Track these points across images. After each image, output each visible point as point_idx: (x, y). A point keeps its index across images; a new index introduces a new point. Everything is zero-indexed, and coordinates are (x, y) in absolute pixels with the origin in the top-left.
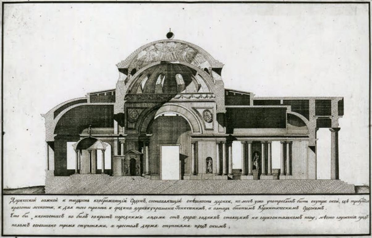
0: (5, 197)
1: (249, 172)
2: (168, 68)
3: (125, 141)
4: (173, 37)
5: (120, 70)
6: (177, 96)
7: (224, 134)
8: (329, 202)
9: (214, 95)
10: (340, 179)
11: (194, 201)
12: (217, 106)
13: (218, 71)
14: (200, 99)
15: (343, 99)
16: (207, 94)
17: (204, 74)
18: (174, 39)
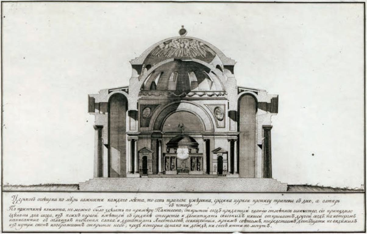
1: (160, 170)
4: (186, 34)
5: (134, 66)
8: (81, 201)
10: (273, 176)
11: (71, 200)
12: (228, 103)
13: (231, 68)
15: (278, 96)
17: (217, 71)
18: (186, 36)
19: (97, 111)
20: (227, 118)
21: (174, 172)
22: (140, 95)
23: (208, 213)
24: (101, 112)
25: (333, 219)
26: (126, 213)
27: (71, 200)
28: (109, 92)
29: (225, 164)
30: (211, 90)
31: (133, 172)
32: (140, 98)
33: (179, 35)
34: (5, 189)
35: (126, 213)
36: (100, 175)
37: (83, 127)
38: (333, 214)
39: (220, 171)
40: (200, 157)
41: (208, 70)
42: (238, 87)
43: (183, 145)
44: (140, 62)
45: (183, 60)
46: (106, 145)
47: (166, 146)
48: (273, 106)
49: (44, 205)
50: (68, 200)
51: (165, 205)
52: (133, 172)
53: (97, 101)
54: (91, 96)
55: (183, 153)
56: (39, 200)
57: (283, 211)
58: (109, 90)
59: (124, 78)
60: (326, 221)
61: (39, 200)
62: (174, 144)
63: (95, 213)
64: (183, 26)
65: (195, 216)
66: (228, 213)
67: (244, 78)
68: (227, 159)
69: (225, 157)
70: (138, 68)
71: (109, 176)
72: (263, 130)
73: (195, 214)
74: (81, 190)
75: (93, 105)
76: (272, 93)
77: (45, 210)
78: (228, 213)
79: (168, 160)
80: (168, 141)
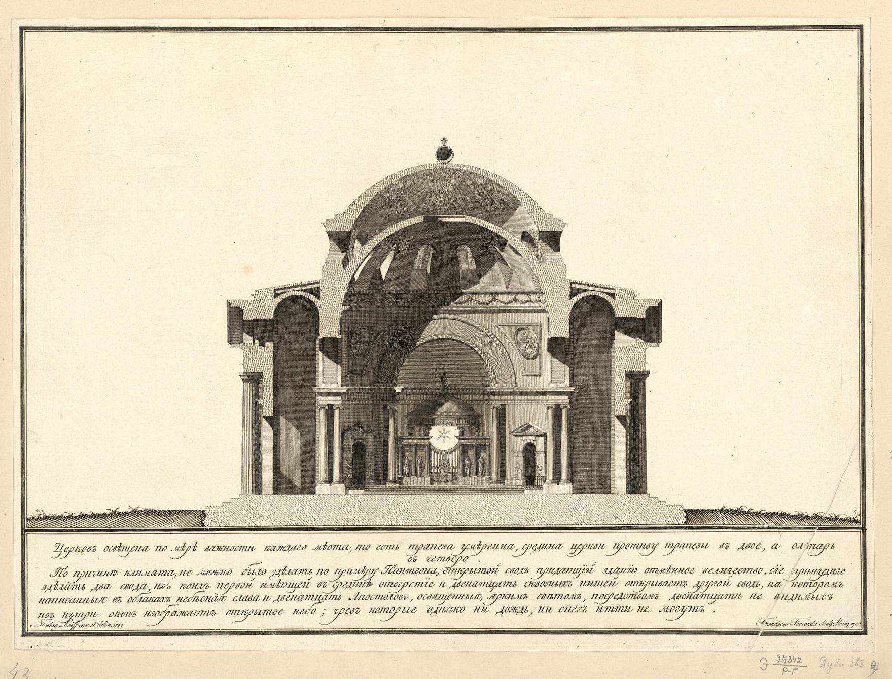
0: (31, 538)
1: (391, 476)
2: (444, 239)
3: (571, 403)
5: (333, 236)
6: (463, 298)
7: (565, 386)
9: (542, 298)
13: (552, 239)
14: (493, 304)
15: (660, 304)
16: (529, 293)
19: (247, 338)
20: (546, 356)
21: (426, 481)
22: (344, 304)
23: (501, 577)
24: (257, 342)
25: (804, 591)
26: (317, 579)
27: (183, 548)
28: (276, 295)
29: (539, 460)
30: (509, 290)
31: (329, 481)
32: (346, 308)
33: (434, 161)
34: (28, 525)
35: (317, 579)
36: (258, 490)
37: (219, 379)
38: (803, 578)
39: (530, 479)
40: (485, 446)
41: (502, 243)
42: (571, 283)
43: (446, 420)
44: (346, 226)
45: (444, 220)
46: (268, 419)
47: (406, 420)
48: (648, 326)
49: (114, 561)
50: (177, 549)
51: (400, 559)
52: (329, 481)
53: (247, 317)
54: (233, 305)
55: (444, 435)
56: (107, 549)
57: (675, 571)
58: (275, 290)
59: (306, 261)
60: (100, 549)
61: (107, 549)
62: (423, 418)
63: (247, 579)
64: (444, 140)
65: (469, 584)
66: (548, 577)
67: (586, 261)
68: (545, 452)
69: (539, 444)
70: (341, 240)
71: (276, 492)
72: (629, 381)
73: (467, 577)
74: (209, 523)
75: (239, 324)
76: (648, 294)
77: (127, 573)
78: (548, 577)
79: (409, 455)
80: (407, 409)
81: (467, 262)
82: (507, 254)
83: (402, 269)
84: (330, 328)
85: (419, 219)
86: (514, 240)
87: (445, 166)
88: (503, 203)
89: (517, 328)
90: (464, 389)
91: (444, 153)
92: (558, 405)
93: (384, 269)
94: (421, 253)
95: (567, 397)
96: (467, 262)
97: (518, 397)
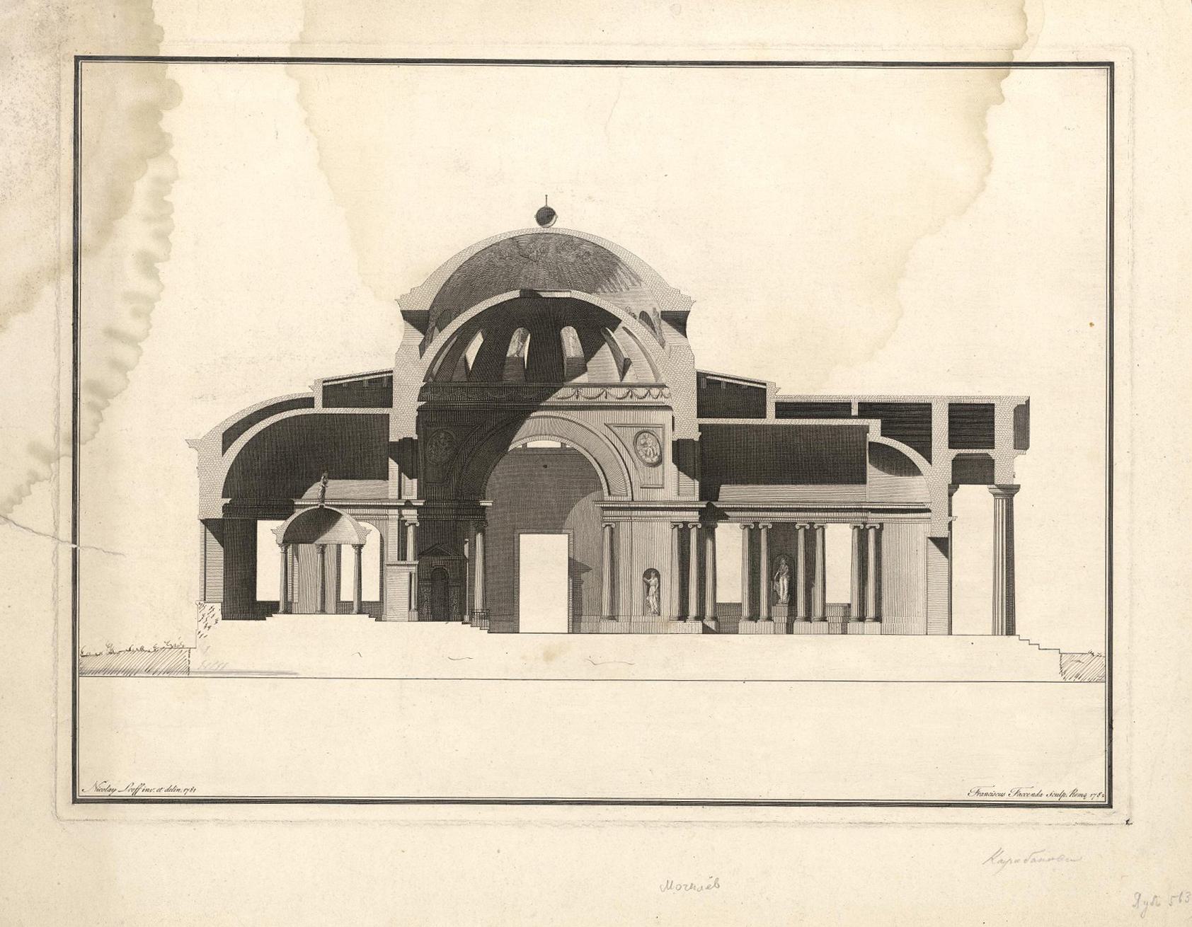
2: (543, 317)
5: (409, 316)
9: (665, 391)
13: (678, 321)
20: (670, 467)
33: (535, 226)
41: (614, 322)
45: (544, 295)
70: (418, 320)
81: (571, 341)
82: (618, 335)
83: (494, 352)
84: (403, 421)
85: (515, 294)
86: (627, 321)
87: (546, 230)
88: (602, 264)
89: (636, 430)
90: (567, 486)
91: (546, 216)
92: (685, 523)
93: (472, 353)
94: (516, 337)
95: (696, 513)
96: (571, 341)
97: (635, 513)
